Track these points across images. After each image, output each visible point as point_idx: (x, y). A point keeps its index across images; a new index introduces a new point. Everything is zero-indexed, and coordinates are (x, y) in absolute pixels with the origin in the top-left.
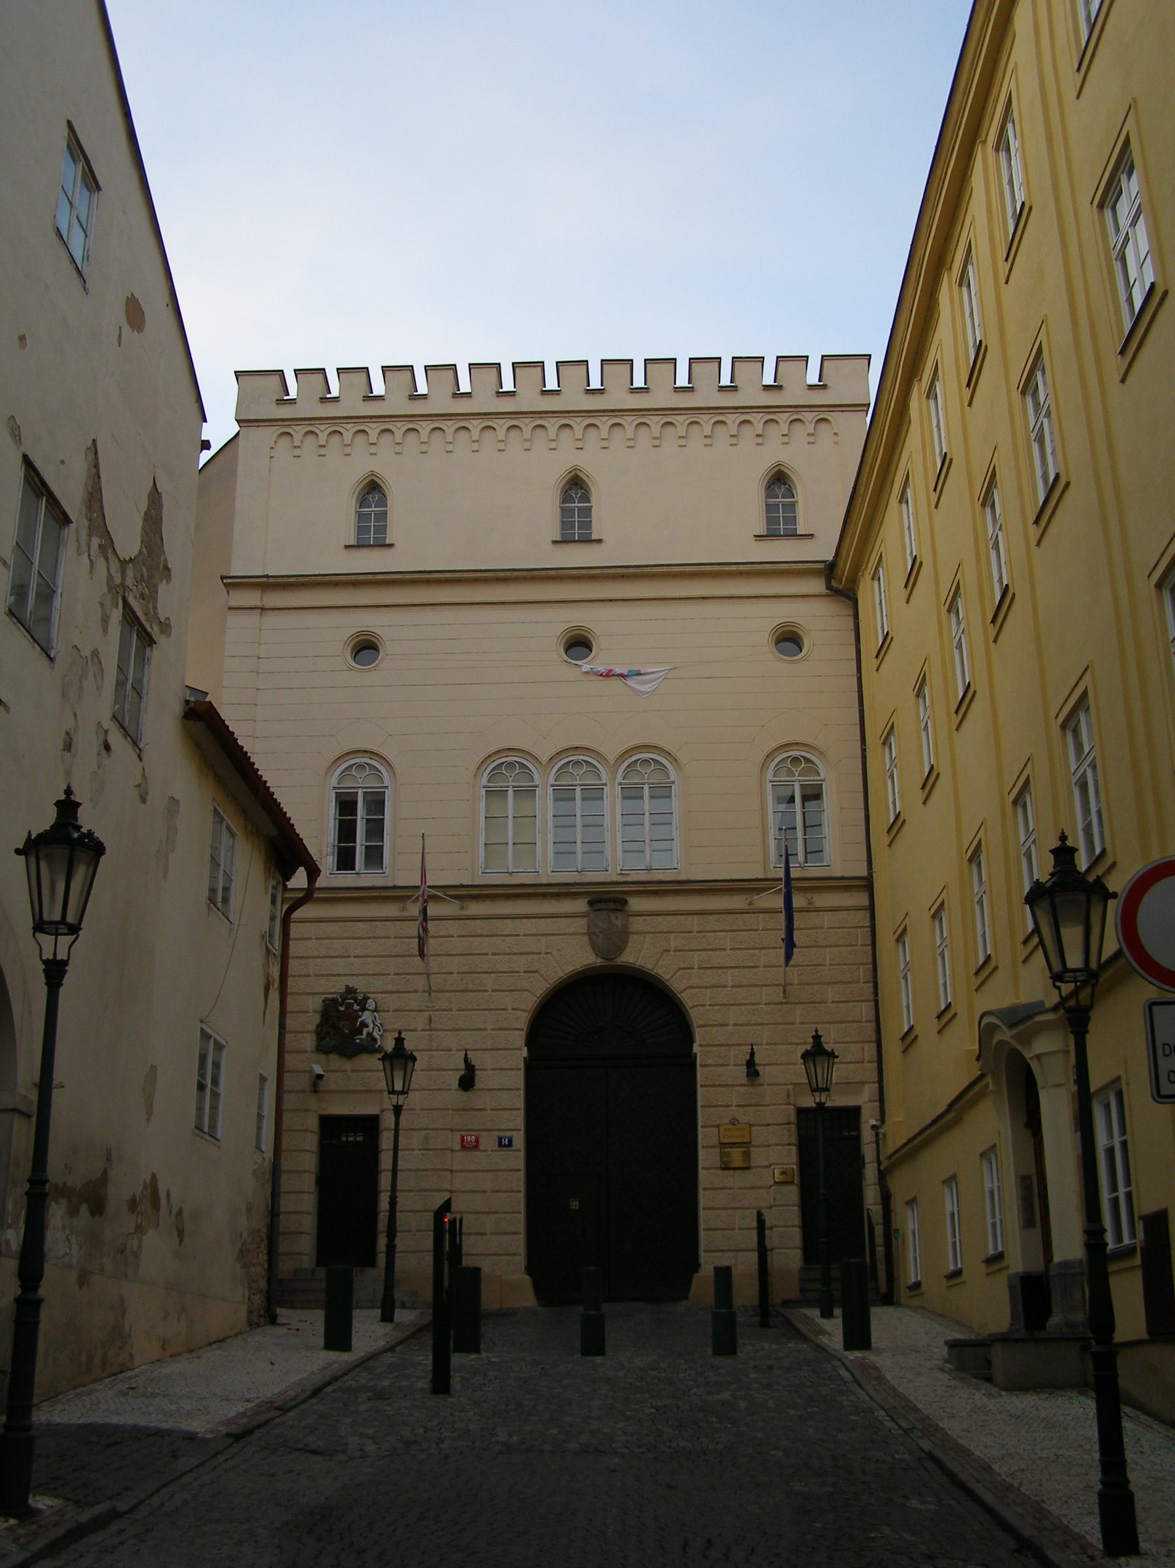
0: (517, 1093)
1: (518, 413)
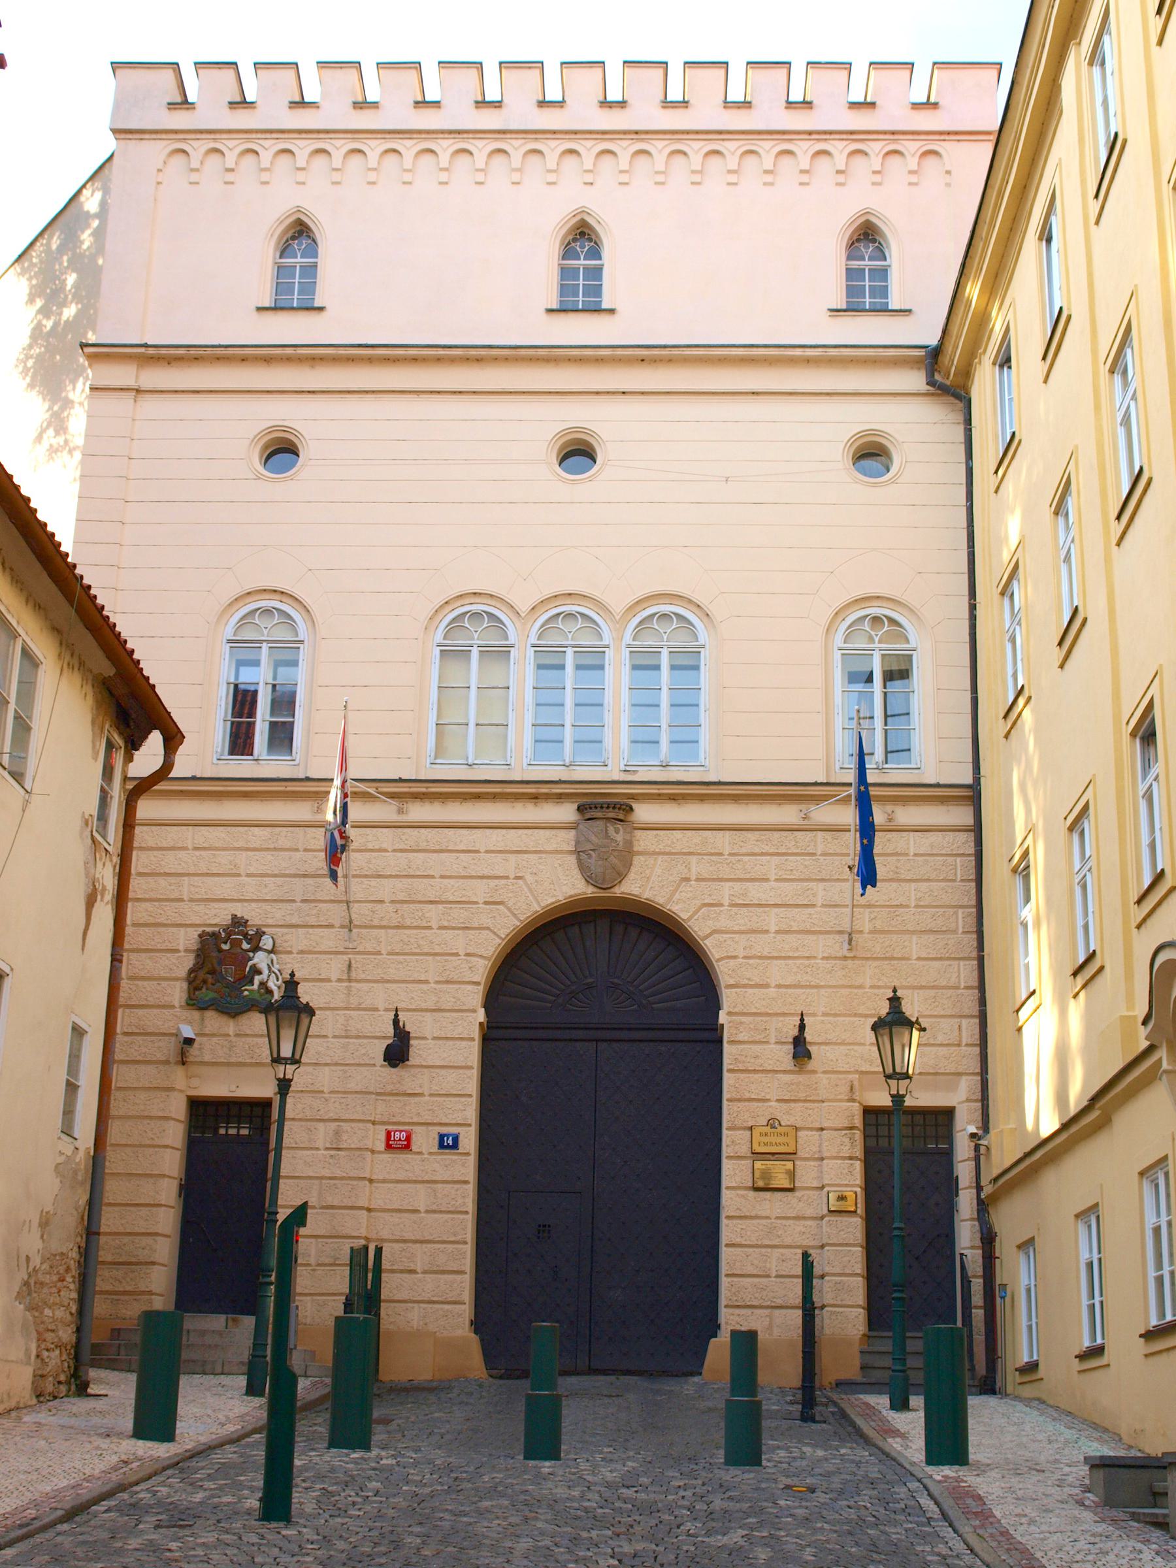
0: (468, 1072)
1: (504, 132)
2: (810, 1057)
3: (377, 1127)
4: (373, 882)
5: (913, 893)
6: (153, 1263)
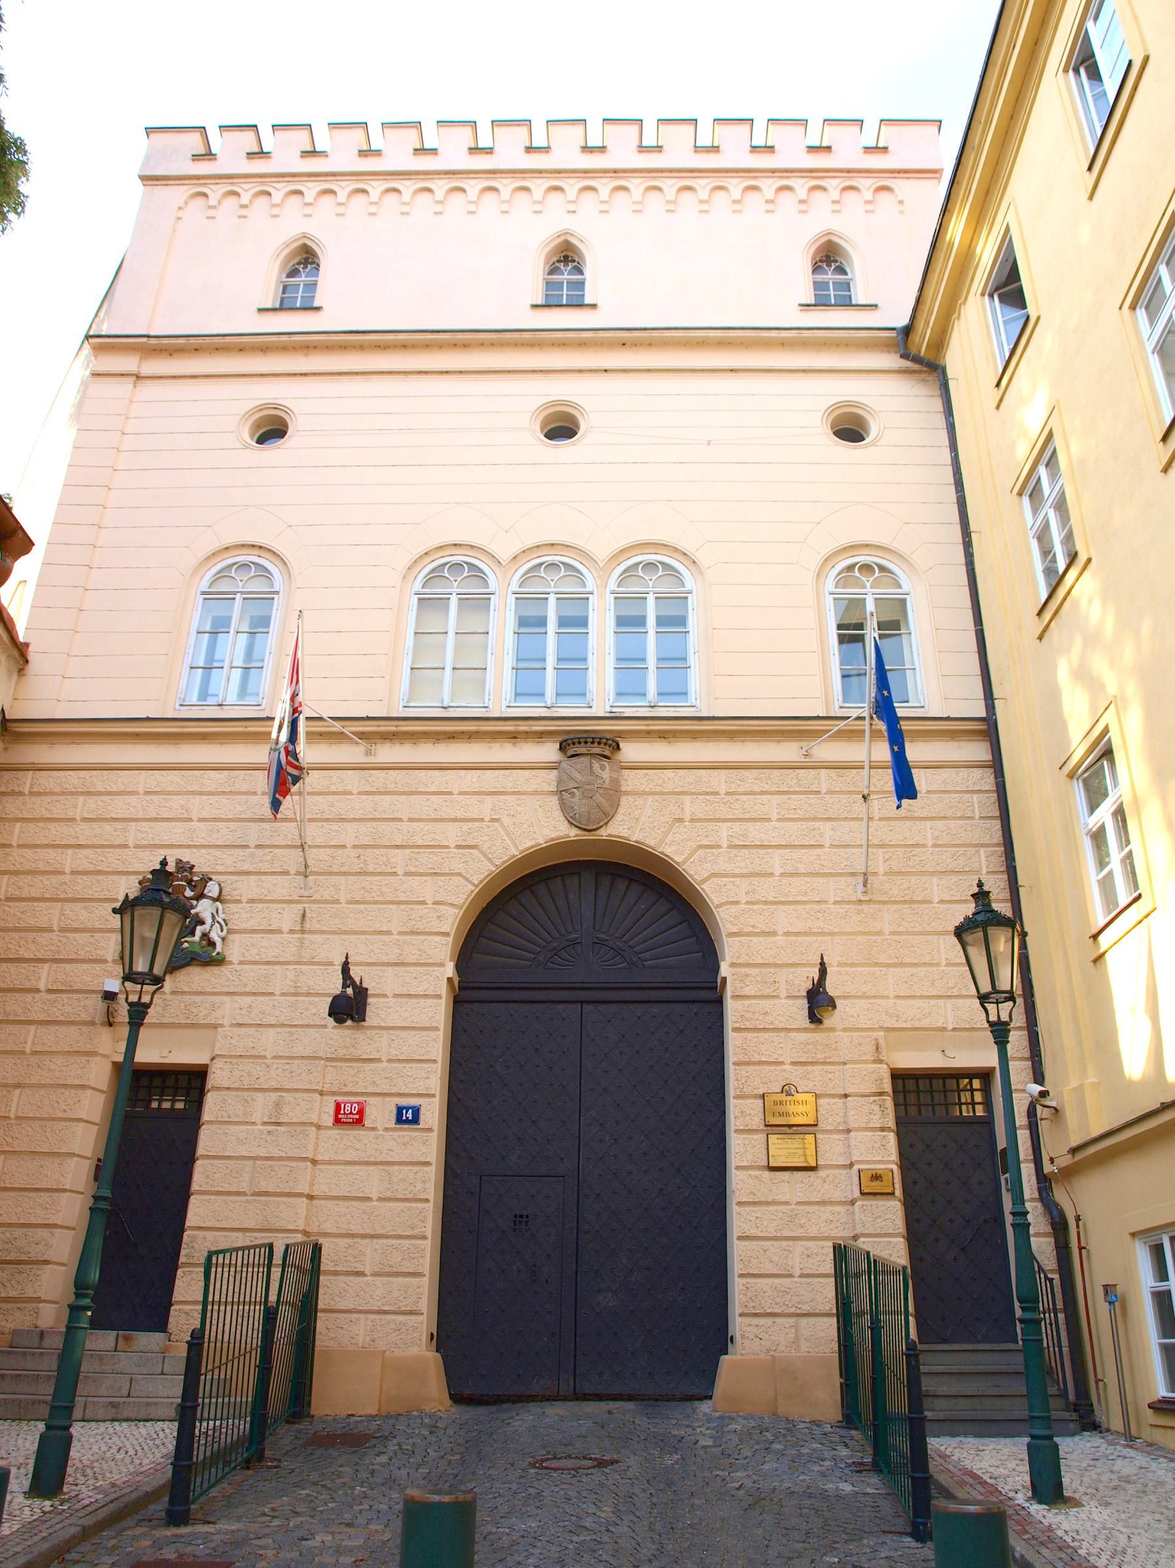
2: (834, 1007)
3: (325, 1098)
4: (335, 826)
5: (929, 831)
6: (47, 1262)
